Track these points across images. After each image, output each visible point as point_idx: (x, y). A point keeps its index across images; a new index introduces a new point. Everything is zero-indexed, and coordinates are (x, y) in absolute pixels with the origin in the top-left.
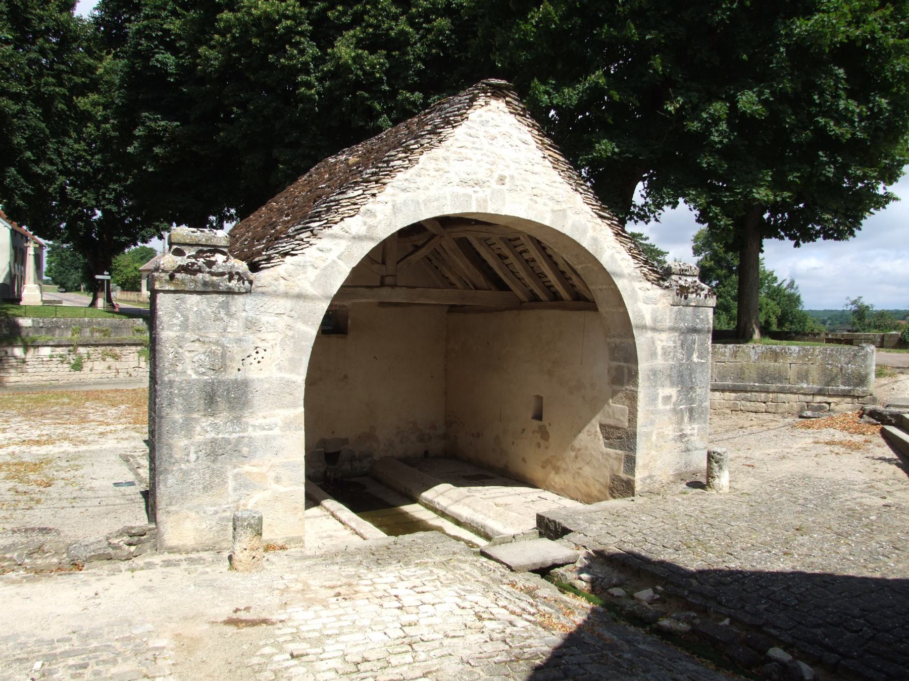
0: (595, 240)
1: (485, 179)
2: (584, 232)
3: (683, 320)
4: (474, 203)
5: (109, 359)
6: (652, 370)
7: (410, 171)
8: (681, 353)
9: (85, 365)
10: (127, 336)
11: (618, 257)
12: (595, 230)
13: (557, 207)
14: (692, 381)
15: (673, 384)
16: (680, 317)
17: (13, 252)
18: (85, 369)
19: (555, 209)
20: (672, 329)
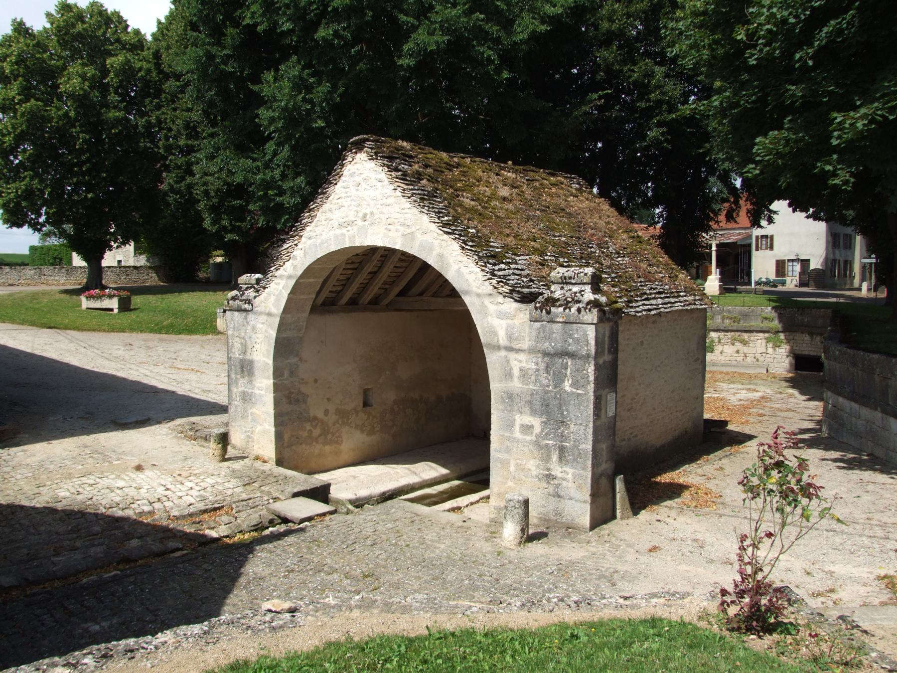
0: (441, 256)
1: (353, 219)
2: (431, 249)
3: (549, 338)
4: (347, 240)
5: (737, 344)
6: (506, 392)
7: (313, 224)
8: (546, 378)
9: (715, 348)
10: (755, 323)
11: (465, 271)
12: (441, 247)
13: (409, 231)
14: (562, 414)
15: (534, 413)
16: (542, 336)
17: (830, 239)
18: (716, 351)
19: (405, 233)
20: (531, 351)
